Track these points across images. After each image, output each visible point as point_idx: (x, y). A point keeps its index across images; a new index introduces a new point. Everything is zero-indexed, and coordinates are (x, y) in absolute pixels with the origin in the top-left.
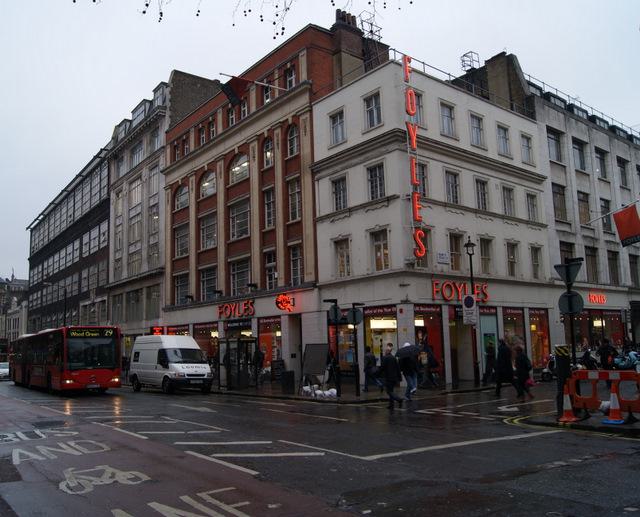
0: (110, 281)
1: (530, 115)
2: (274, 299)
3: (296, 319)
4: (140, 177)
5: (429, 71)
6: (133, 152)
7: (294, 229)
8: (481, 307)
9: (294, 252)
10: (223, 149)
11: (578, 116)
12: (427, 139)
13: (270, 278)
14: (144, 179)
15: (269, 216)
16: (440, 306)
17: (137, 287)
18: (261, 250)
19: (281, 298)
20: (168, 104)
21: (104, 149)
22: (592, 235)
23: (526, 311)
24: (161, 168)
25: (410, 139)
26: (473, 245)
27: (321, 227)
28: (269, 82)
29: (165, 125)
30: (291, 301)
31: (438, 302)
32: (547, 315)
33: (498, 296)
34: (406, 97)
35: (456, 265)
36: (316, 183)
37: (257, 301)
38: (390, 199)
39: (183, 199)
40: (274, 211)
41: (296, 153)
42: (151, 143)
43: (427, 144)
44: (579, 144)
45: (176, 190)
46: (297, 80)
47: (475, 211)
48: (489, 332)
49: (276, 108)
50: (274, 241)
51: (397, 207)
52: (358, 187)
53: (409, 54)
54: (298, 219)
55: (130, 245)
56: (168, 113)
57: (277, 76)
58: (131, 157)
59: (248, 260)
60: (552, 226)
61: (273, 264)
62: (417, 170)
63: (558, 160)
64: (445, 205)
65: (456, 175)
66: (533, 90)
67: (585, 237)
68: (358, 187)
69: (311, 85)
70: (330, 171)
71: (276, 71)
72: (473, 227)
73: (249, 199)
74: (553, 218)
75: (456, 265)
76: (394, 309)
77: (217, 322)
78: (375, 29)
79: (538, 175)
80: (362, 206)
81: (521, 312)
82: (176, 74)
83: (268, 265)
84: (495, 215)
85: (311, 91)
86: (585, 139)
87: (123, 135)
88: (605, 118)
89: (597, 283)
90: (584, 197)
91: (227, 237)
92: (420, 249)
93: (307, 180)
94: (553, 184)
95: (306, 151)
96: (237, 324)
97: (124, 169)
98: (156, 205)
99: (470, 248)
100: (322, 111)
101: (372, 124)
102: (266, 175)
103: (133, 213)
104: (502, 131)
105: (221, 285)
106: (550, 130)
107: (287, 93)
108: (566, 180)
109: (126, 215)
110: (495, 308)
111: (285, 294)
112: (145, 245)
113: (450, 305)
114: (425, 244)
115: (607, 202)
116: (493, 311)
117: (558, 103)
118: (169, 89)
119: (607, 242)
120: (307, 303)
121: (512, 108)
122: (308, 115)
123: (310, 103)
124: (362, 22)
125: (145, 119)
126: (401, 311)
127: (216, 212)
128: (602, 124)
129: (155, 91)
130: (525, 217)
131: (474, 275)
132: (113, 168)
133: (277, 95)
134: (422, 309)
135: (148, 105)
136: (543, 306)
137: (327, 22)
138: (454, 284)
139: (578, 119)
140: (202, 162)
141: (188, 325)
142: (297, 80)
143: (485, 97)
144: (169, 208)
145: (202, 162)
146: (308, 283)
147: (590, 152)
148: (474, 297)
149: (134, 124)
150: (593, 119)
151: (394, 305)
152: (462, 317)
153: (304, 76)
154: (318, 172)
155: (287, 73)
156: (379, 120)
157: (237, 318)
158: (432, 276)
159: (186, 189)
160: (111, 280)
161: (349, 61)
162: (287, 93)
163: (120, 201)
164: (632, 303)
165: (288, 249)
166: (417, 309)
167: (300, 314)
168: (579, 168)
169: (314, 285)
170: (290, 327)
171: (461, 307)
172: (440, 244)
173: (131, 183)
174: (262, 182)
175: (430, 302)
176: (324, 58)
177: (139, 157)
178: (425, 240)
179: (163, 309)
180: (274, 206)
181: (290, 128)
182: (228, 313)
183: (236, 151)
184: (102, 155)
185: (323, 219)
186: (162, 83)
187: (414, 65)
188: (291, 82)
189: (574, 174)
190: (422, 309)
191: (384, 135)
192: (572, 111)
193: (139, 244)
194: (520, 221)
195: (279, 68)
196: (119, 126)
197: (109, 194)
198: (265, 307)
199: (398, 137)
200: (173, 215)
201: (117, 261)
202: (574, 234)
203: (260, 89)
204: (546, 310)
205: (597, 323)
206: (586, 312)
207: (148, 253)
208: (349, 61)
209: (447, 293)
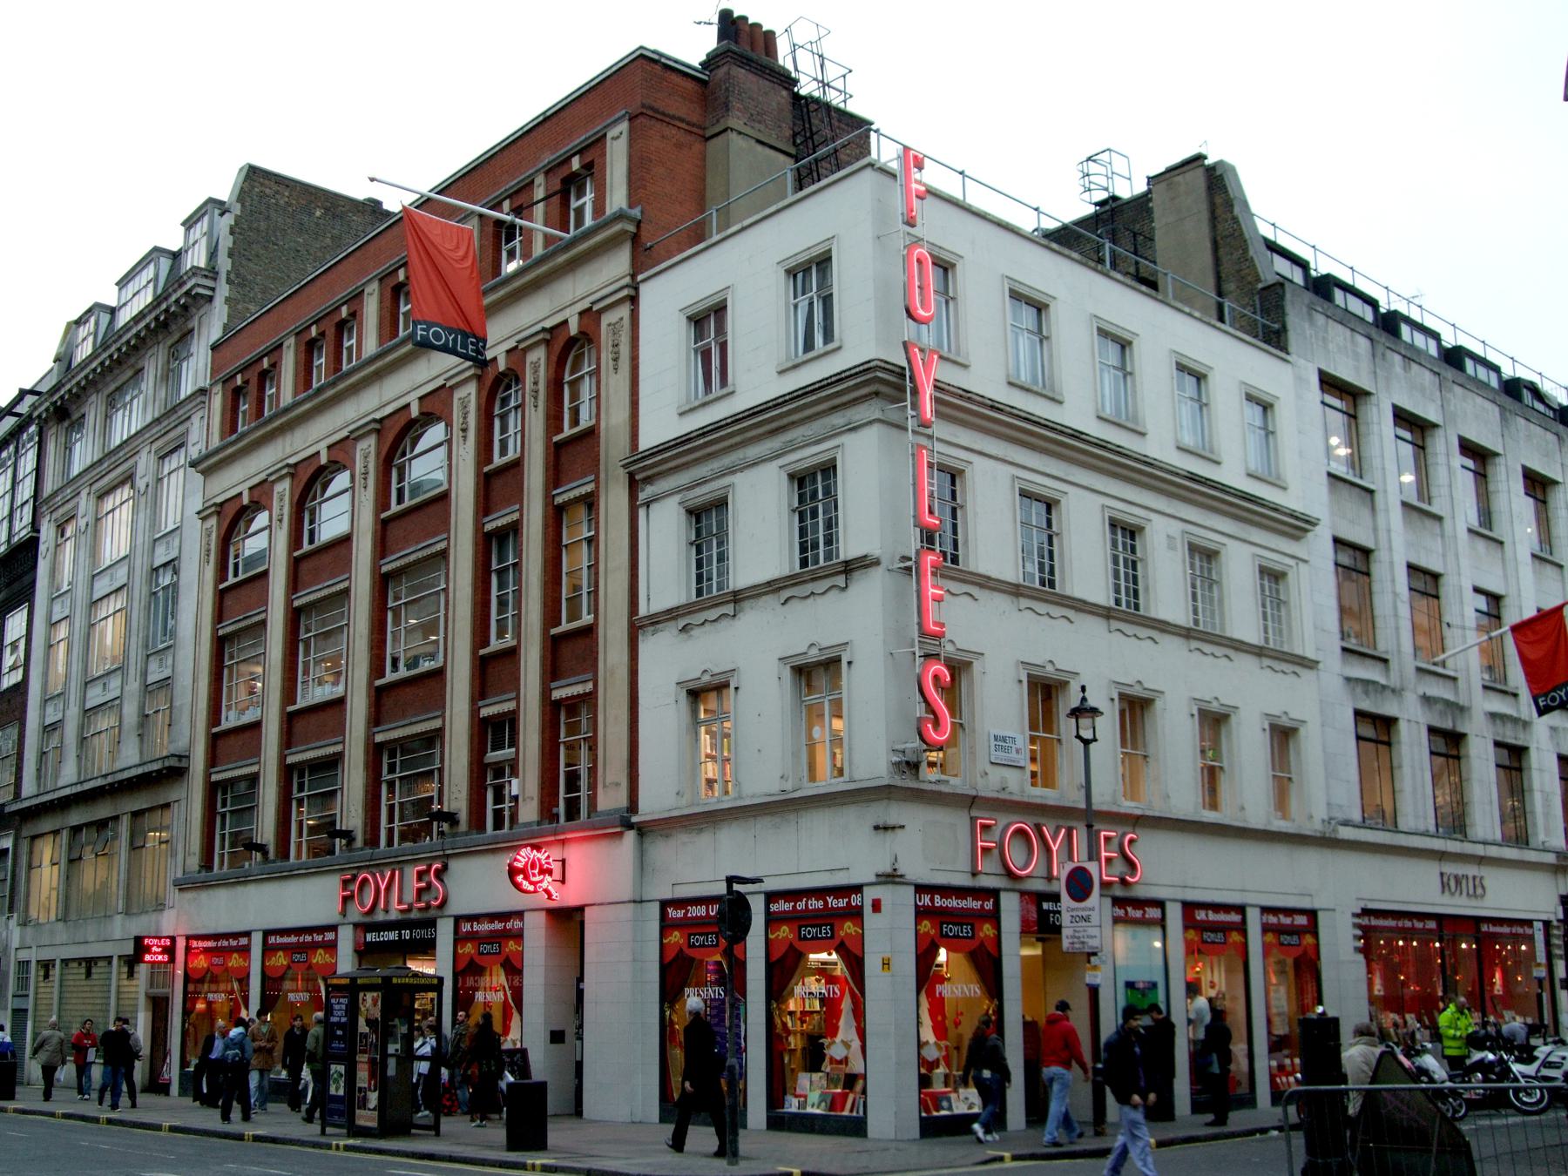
0: (25, 792)
1: (1274, 338)
2: (505, 860)
4: (129, 478)
5: (978, 198)
6: (112, 404)
8: (1118, 902)
11: (1412, 346)
12: (966, 395)
13: (499, 798)
14: (141, 483)
15: (502, 603)
16: (994, 894)
17: (102, 811)
18: (474, 711)
19: (525, 856)
20: (224, 264)
21: (32, 392)
22: (1449, 696)
23: (1254, 921)
24: (194, 452)
26: (1094, 712)
27: (649, 646)
28: (517, 211)
29: (213, 325)
30: (556, 867)
32: (1313, 928)
34: (907, 269)
35: (1044, 776)
36: (642, 512)
37: (454, 865)
38: (850, 568)
39: (253, 545)
40: (518, 593)
41: (585, 421)
42: (170, 376)
44: (1478, 455)
47: (1106, 614)
48: (1141, 977)
49: (537, 285)
50: (513, 683)
51: (870, 591)
53: (919, 146)
54: (587, 619)
55: (88, 683)
56: (223, 290)
57: (539, 193)
58: (108, 417)
59: (433, 739)
60: (1334, 666)
61: (508, 752)
62: (932, 484)
63: (1420, 497)
64: (1015, 591)
65: (1050, 505)
66: (1282, 266)
67: (1427, 700)
69: (638, 224)
70: (683, 478)
71: (540, 179)
73: (444, 554)
74: (1336, 644)
75: (1044, 776)
76: (855, 900)
77: (333, 928)
78: (832, 73)
79: (1292, 514)
80: (773, 587)
81: (1234, 917)
82: (254, 176)
83: (493, 756)
84: (1163, 627)
85: (635, 239)
86: (1430, 413)
87: (84, 351)
88: (1492, 357)
89: (1395, 829)
90: (1426, 582)
91: (377, 669)
92: (937, 722)
93: (615, 500)
94: (1337, 541)
95: (615, 419)
96: (392, 936)
97: (84, 453)
98: (172, 565)
99: (1084, 722)
101: (809, 345)
103: (103, 586)
104: (1190, 381)
105: (351, 812)
106: (1329, 383)
108: (1375, 529)
109: (81, 592)
110: (1160, 904)
111: (537, 847)
112: (134, 686)
113: (1023, 893)
114: (954, 708)
115: (1495, 599)
116: (1153, 913)
117: (1355, 306)
118: (228, 220)
119: (1494, 716)
121: (1221, 319)
122: (624, 311)
123: (633, 276)
124: (794, 48)
125: (158, 301)
126: (877, 906)
127: (346, 591)
128: (1482, 373)
129: (189, 224)
130: (1252, 636)
131: (1095, 807)
132: (51, 447)
133: (538, 249)
135: (165, 264)
136: (1305, 903)
138: (1038, 829)
139: (1412, 356)
140: (313, 439)
141: (247, 934)
143: (1148, 283)
144: (210, 573)
145: (313, 439)
146: (609, 813)
147: (1444, 447)
148: (1092, 868)
149: (124, 317)
150: (1455, 357)
151: (858, 889)
152: (1060, 927)
153: (617, 198)
154: (649, 480)
155: (570, 185)
156: (828, 335)
157: (394, 915)
158: (971, 801)
159: (262, 519)
160: (29, 788)
163: (69, 546)
165: (552, 710)
166: (926, 900)
167: (580, 909)
168: (1474, 523)
169: (628, 821)
171: (1056, 898)
173: (101, 496)
174: (485, 504)
176: (679, 146)
177: (128, 422)
178: (951, 691)
180: (518, 581)
184: (23, 408)
185: (656, 620)
186: (211, 201)
187: (932, 176)
188: (580, 212)
189: (1396, 514)
191: (839, 378)
192: (1395, 333)
193: (115, 682)
194: (1239, 646)
195: (549, 172)
196: (79, 322)
197: (35, 526)
200: (221, 596)
201: (49, 729)
202: (1396, 692)
203: (490, 229)
204: (1312, 914)
206: (1432, 925)
207: (142, 707)
209: (1015, 856)
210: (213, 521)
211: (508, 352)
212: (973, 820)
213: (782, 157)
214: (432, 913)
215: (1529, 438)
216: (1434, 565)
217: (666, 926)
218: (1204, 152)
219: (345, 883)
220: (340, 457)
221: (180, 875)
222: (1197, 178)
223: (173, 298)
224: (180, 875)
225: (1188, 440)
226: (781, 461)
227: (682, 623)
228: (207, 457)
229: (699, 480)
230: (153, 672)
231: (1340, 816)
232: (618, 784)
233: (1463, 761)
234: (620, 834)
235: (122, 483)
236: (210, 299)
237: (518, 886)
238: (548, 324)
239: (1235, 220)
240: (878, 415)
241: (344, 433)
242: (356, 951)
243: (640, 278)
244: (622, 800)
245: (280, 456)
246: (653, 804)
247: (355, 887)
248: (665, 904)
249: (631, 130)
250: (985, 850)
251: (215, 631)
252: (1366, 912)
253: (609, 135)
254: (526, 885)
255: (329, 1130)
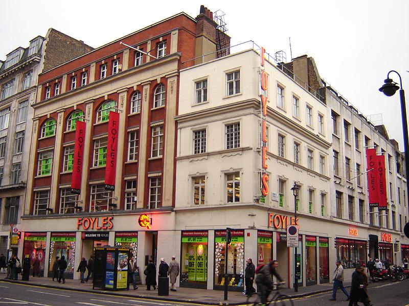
1: (323, 100)
2: (137, 218)
3: (152, 237)
7: (155, 165)
9: (155, 183)
10: (93, 95)
16: (272, 232)
18: (123, 179)
19: (143, 217)
20: (44, 54)
23: (318, 238)
24: (31, 103)
25: (263, 107)
29: (39, 69)
30: (150, 220)
31: (271, 229)
33: (304, 227)
36: (179, 131)
37: (115, 218)
38: (243, 150)
43: (272, 114)
45: (43, 121)
46: (168, 51)
52: (216, 138)
54: (159, 156)
56: (43, 60)
60: (333, 179)
61: (133, 189)
68: (216, 138)
69: (180, 57)
72: (293, 176)
77: (75, 232)
82: (53, 31)
83: (127, 190)
85: (179, 61)
95: (171, 106)
98: (23, 132)
100: (189, 78)
102: (133, 120)
107: (157, 60)
111: (146, 215)
113: (277, 232)
118: (45, 42)
120: (160, 222)
122: (175, 79)
125: (21, 62)
126: (248, 235)
129: (32, 41)
133: (148, 60)
134: (195, 233)
135: (22, 51)
137: (194, 13)
138: (281, 216)
141: (46, 232)
142: (168, 51)
144: (35, 135)
149: (7, 66)
153: (174, 49)
157: (95, 230)
158: (269, 209)
161: (207, 45)
162: (157, 60)
164: (370, 236)
167: (157, 231)
169: (172, 209)
170: (145, 238)
171: (286, 234)
172: (273, 187)
175: (266, 229)
179: (21, 217)
181: (158, 86)
182: (87, 225)
183: (106, 98)
190: (195, 233)
198: (124, 223)
199: (256, 105)
204: (328, 238)
205: (201, 248)
208: (207, 45)
210: (38, 121)
211: (138, 85)
212: (269, 214)
213: (214, 44)
214: (108, 230)
215: (366, 129)
216: (349, 158)
217: (183, 236)
218: (306, 54)
219: (79, 221)
220: (81, 108)
221: (22, 215)
222: (305, 61)
223: (28, 61)
224: (22, 215)
225: (309, 125)
226: (223, 121)
227: (191, 160)
228: (36, 104)
229: (198, 124)
230: (15, 160)
231: (333, 215)
232: (169, 200)
233: (353, 203)
234: (170, 213)
235: (7, 109)
236: (39, 62)
237: (141, 225)
238: (151, 79)
239: (314, 71)
240: (253, 112)
241: (83, 102)
242: (82, 239)
243: (180, 71)
244: (170, 204)
245: (60, 106)
246: (178, 206)
247: (83, 222)
248: (183, 231)
249: (179, 32)
250: (271, 221)
251: (36, 151)
252: (337, 238)
253: (172, 33)
254: (143, 225)
255: (95, 288)
